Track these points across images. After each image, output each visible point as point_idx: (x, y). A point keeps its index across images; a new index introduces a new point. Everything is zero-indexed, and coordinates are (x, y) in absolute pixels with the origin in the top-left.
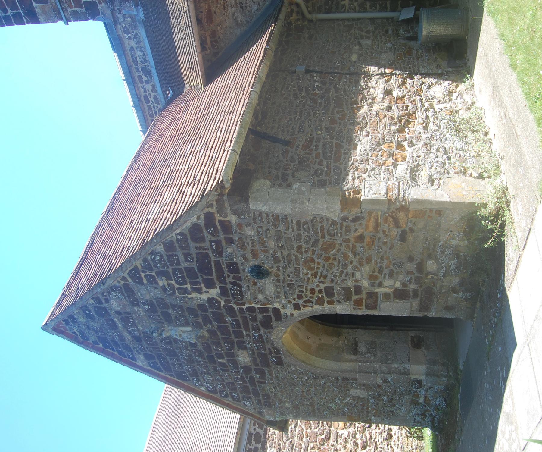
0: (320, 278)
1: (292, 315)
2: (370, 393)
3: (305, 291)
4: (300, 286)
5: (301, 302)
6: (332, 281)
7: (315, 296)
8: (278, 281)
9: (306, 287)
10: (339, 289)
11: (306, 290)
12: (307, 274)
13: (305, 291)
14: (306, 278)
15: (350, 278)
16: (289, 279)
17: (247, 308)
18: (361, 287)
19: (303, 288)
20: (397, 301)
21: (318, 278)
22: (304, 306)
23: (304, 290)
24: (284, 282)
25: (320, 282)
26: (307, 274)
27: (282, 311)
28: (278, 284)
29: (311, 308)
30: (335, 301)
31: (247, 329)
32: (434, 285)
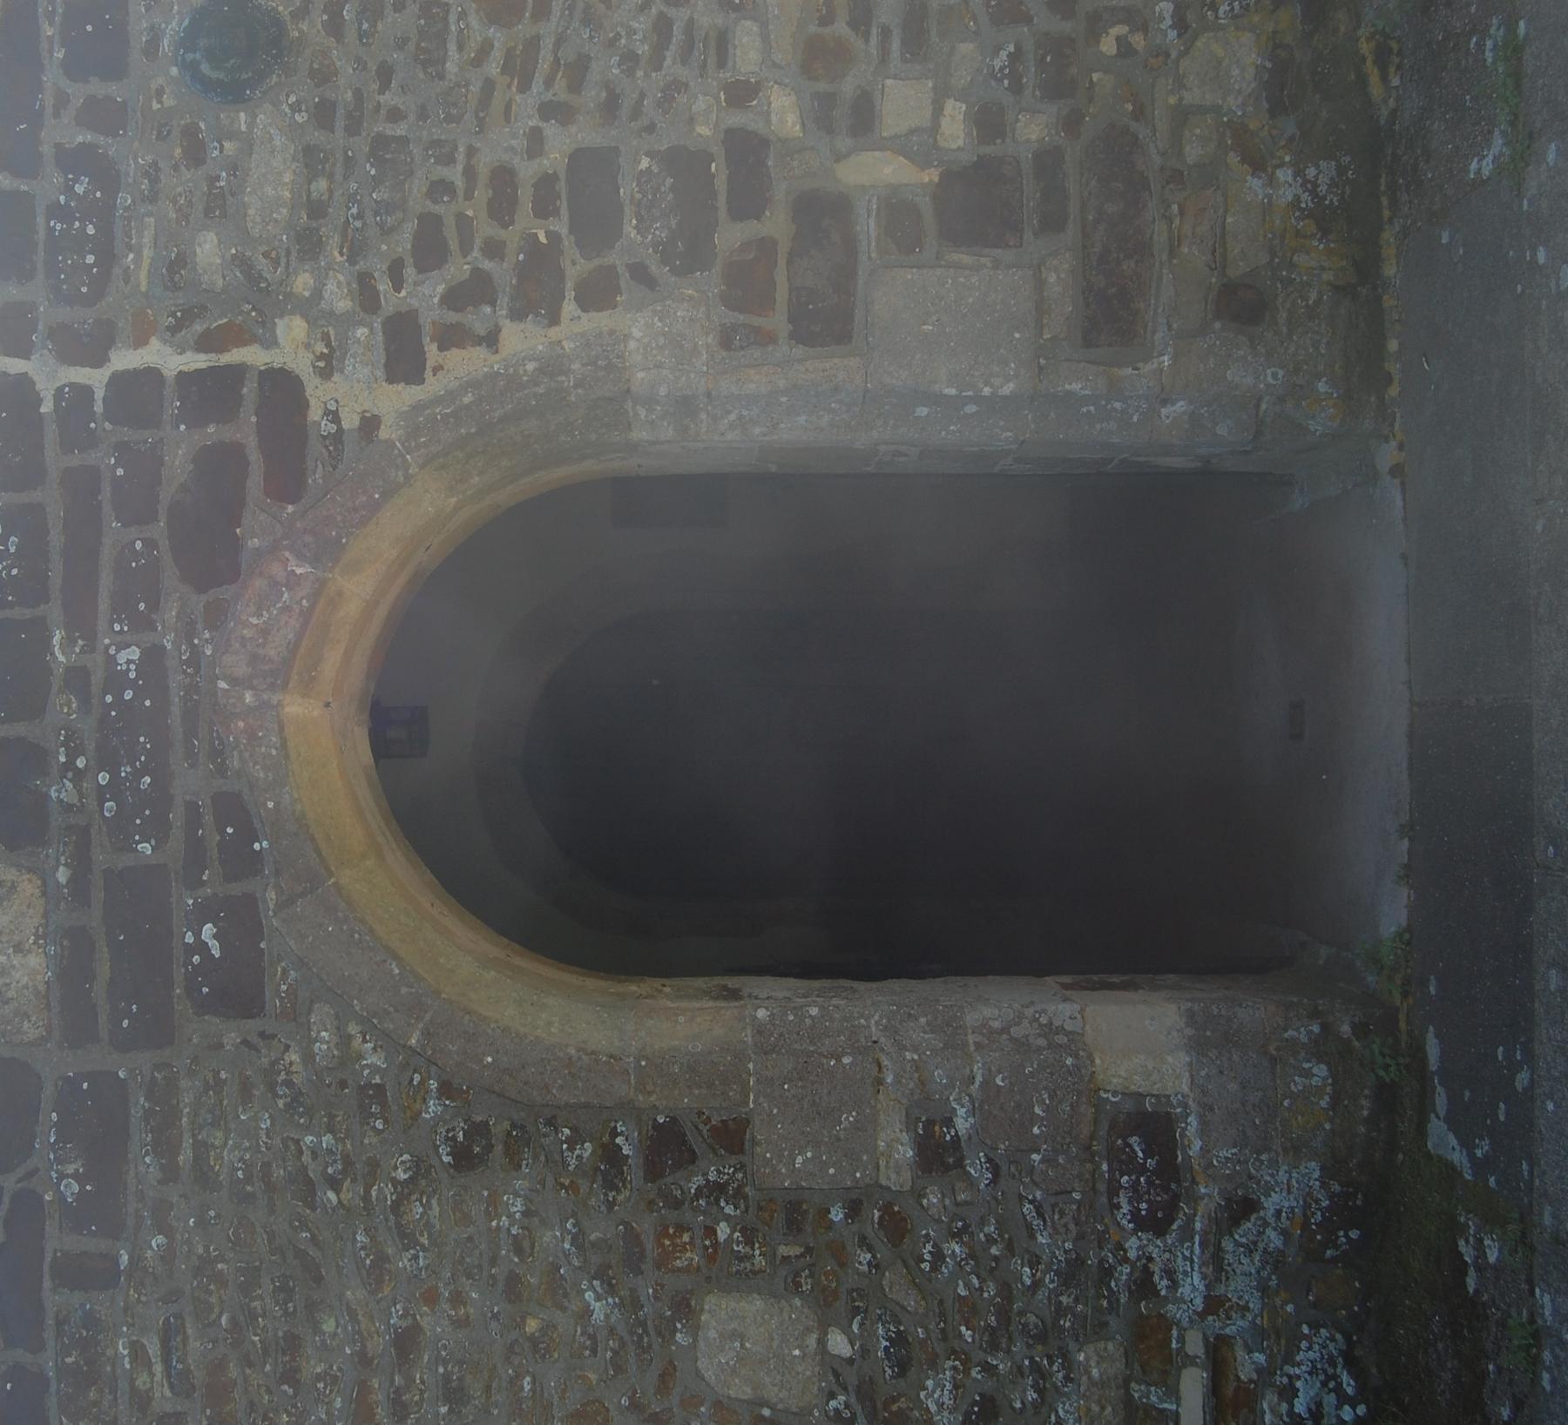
0: (549, 82)
1: (370, 424)
2: (839, 1344)
3: (459, 183)
4: (436, 143)
5: (425, 295)
6: (610, 107)
7: (512, 236)
8: (324, 114)
9: (471, 152)
10: (645, 163)
11: (470, 173)
12: (485, 50)
13: (459, 183)
14: (475, 88)
15: (704, 66)
16: (387, 99)
17: (120, 381)
18: (764, 143)
19: (449, 160)
20: (956, 257)
21: (537, 86)
22: (451, 337)
23: (455, 175)
24: (353, 129)
25: (548, 111)
26: (485, 50)
27: (318, 394)
28: (317, 137)
29: (480, 352)
30: (625, 279)
31: (81, 624)
32: (1139, 114)
